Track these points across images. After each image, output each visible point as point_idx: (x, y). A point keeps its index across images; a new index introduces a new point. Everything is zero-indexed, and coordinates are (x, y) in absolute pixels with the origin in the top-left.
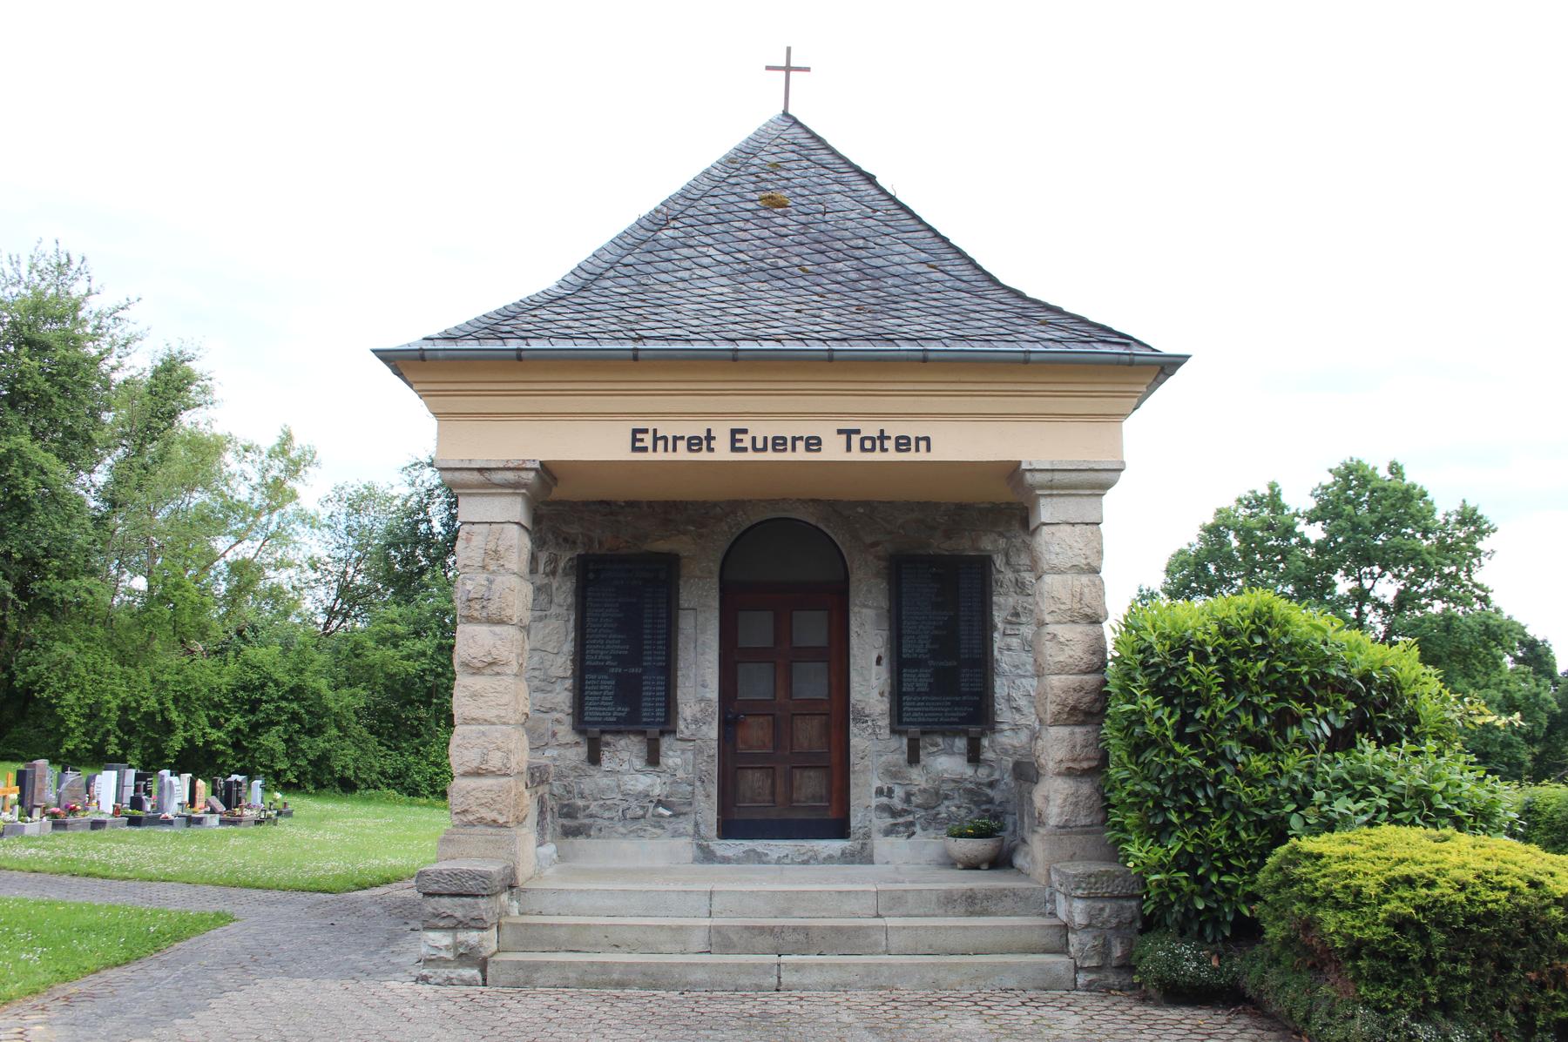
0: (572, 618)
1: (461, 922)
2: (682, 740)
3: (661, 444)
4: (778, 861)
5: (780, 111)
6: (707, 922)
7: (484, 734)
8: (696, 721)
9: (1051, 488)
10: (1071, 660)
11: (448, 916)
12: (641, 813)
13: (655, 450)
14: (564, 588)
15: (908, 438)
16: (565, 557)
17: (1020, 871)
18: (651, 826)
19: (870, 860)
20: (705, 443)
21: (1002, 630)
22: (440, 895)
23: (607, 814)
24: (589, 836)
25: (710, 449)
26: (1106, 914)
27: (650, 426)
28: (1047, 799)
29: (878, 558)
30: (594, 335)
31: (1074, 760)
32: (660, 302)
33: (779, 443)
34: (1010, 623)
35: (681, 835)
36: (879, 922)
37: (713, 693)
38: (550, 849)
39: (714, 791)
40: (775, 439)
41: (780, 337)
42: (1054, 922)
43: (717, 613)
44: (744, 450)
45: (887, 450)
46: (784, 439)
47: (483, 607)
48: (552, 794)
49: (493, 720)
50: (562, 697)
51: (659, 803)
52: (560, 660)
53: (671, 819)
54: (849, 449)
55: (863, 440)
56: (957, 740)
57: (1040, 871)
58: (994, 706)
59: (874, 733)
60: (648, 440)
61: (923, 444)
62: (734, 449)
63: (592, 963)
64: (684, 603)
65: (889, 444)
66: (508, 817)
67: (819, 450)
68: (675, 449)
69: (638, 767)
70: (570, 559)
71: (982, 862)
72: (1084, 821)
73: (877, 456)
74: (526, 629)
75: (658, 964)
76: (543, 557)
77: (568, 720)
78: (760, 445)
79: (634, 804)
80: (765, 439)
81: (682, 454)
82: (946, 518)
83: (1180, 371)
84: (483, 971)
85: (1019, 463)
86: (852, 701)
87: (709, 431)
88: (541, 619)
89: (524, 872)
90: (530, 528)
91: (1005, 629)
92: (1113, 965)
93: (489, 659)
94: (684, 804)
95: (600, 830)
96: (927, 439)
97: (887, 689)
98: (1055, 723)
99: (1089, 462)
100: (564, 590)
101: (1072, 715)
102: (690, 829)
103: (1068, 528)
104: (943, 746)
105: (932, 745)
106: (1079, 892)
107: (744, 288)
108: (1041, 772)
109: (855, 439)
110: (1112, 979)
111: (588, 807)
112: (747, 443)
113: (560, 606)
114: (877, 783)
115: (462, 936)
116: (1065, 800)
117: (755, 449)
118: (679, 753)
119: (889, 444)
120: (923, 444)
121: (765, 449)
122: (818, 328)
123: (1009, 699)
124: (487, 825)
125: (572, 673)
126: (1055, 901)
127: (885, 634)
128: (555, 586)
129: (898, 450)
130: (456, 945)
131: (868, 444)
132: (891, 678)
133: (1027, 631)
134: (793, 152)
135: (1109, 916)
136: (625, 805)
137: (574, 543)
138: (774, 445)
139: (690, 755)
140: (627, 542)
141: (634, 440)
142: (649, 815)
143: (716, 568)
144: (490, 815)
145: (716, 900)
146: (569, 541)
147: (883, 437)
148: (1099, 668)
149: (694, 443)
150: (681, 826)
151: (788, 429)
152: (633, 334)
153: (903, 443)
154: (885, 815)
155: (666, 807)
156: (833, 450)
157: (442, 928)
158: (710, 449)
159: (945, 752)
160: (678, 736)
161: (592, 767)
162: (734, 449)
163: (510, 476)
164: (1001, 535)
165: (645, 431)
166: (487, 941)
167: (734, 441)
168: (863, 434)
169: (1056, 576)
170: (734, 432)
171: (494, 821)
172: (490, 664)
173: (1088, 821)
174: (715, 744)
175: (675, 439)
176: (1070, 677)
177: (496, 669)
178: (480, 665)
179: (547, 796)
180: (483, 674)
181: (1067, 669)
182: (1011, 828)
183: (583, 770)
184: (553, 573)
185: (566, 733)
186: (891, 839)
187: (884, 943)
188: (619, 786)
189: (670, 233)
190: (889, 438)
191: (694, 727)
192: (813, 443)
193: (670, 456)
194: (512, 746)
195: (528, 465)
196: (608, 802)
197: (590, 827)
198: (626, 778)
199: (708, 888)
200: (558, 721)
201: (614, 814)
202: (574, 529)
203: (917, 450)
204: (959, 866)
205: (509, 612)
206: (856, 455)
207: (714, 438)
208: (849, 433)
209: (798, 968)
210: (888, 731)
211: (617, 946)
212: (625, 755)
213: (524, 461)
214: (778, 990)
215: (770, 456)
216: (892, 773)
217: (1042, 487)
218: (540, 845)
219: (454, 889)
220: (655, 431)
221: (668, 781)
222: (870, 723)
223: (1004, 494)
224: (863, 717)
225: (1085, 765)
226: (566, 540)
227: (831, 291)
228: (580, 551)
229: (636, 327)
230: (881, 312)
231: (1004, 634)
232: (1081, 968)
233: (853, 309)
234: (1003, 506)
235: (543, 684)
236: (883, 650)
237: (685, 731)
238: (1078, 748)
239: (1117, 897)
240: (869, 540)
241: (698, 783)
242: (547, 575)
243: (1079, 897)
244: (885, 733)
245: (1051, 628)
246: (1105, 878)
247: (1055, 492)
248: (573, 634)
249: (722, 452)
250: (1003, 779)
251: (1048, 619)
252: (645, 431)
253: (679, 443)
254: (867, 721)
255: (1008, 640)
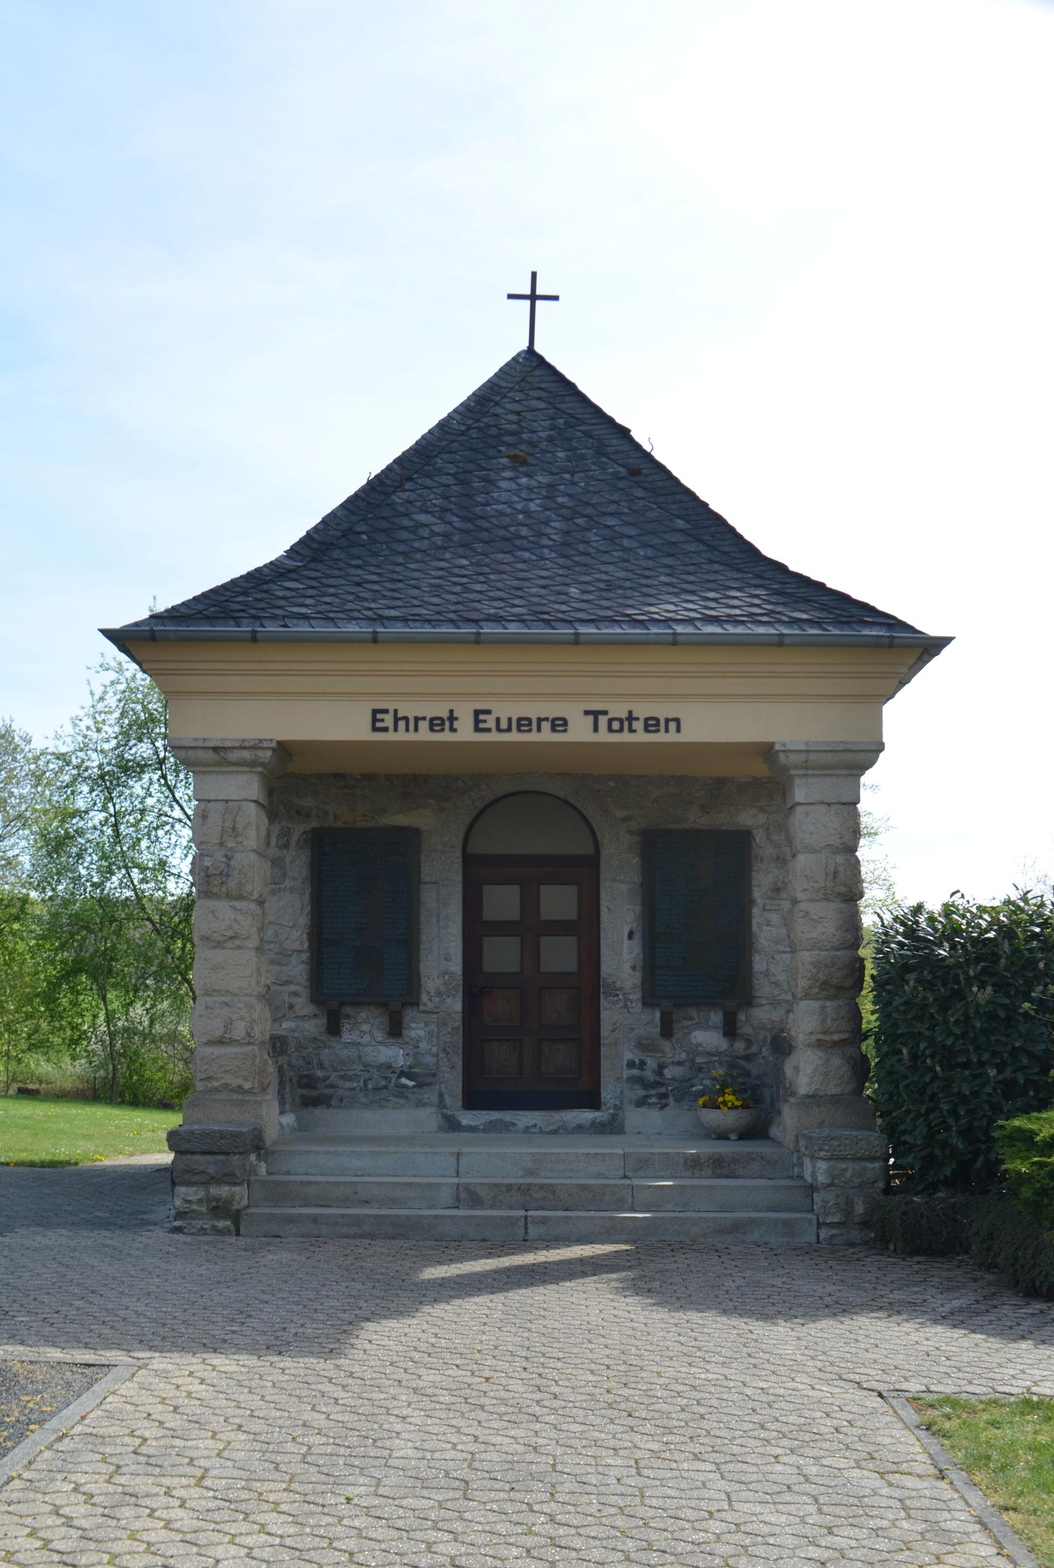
0: (308, 891)
1: (213, 1178)
2: (423, 1012)
3: (402, 724)
4: (527, 1129)
5: (525, 345)
6: (455, 1180)
7: (227, 1004)
8: (439, 994)
9: (806, 768)
10: (824, 937)
11: (201, 1172)
12: (383, 1083)
13: (396, 729)
14: (299, 861)
15: (657, 720)
16: (299, 829)
17: (773, 1140)
18: (394, 1096)
19: (620, 1131)
20: (447, 724)
21: (761, 905)
22: (193, 1153)
23: (347, 1085)
24: (329, 1106)
25: (453, 730)
26: (848, 1174)
27: (391, 707)
28: (797, 1069)
29: (631, 832)
30: (332, 615)
31: (824, 1033)
32: (395, 576)
33: (524, 724)
34: (770, 898)
35: (424, 1105)
36: (627, 1182)
37: (456, 967)
38: (289, 1119)
39: (459, 1063)
40: (519, 720)
41: (525, 617)
42: (799, 1183)
43: (459, 888)
44: (489, 730)
45: (635, 731)
46: (529, 720)
47: (222, 883)
48: (289, 1064)
49: (235, 991)
50: (298, 969)
51: (402, 1074)
52: (296, 934)
53: (415, 1090)
54: (596, 729)
55: (610, 721)
56: (712, 1014)
57: (788, 1139)
58: (751, 981)
59: (626, 1006)
60: (388, 720)
61: (672, 726)
62: (477, 729)
63: (343, 1216)
64: (425, 876)
65: (638, 725)
66: (253, 1083)
67: (565, 731)
68: (416, 729)
69: (380, 1039)
70: (304, 833)
71: (732, 1131)
72: (833, 1090)
73: (626, 737)
74: (261, 903)
75: (407, 1216)
76: (276, 829)
77: (305, 993)
78: (504, 725)
79: (375, 1075)
80: (510, 720)
81: (424, 734)
82: (704, 792)
83: (946, 651)
84: (237, 1224)
85: (772, 745)
86: (603, 974)
87: (451, 712)
88: (274, 892)
89: (271, 1135)
90: (266, 804)
91: (764, 905)
92: (856, 1221)
93: (231, 933)
94: (428, 1075)
95: (341, 1100)
96: (677, 720)
97: (640, 964)
98: (806, 996)
99: (846, 743)
100: (298, 864)
101: (824, 989)
102: (435, 1099)
103: (823, 808)
104: (697, 1020)
105: (685, 1019)
106: (822, 1154)
107: (487, 561)
108: (793, 1044)
109: (603, 720)
110: (855, 1235)
111: (328, 1078)
112: (491, 723)
113: (294, 879)
114: (628, 1056)
115: (214, 1191)
116: (815, 1071)
117: (499, 729)
118: (422, 1025)
119: (638, 725)
120: (672, 726)
121: (509, 729)
122: (564, 608)
123: (767, 974)
124: (232, 1090)
125: (309, 946)
126: (802, 1164)
127: (638, 908)
128: (288, 860)
129: (647, 730)
130: (208, 1199)
131: (616, 725)
132: (644, 952)
133: (786, 905)
134: (539, 399)
135: (852, 1176)
136: (367, 1075)
137: (308, 816)
138: (519, 726)
139: (433, 1027)
140: (364, 815)
141: (374, 720)
142: (392, 1085)
143: (458, 842)
144: (235, 1082)
145: (464, 1161)
146: (302, 814)
147: (631, 718)
148: (853, 945)
149: (436, 724)
150: (426, 1096)
151: (533, 710)
152: (370, 613)
153: (652, 724)
154: (636, 1087)
155: (410, 1077)
156: (580, 731)
157: (194, 1184)
158: (453, 730)
159: (700, 1027)
160: (422, 1008)
161: (332, 1039)
162: (477, 729)
163: (246, 755)
164: (762, 809)
165: (386, 711)
166: (239, 1194)
167: (477, 721)
168: (611, 715)
169: (810, 855)
170: (477, 713)
171: (240, 1087)
172: (231, 938)
173: (838, 1091)
174: (459, 1017)
175: (417, 719)
176: (823, 953)
177: (237, 942)
178: (220, 939)
179: (285, 1066)
180: (224, 948)
181: (819, 945)
182: (768, 1101)
183: (323, 1042)
184: (286, 846)
185: (304, 1005)
186: (643, 1110)
187: (630, 1200)
188: (360, 1057)
189: (405, 495)
190: (637, 719)
191: (437, 999)
192: (559, 724)
193: (411, 736)
194: (256, 1016)
195: (265, 745)
196: (349, 1073)
197: (331, 1097)
198: (368, 1049)
199: (456, 1150)
200: (295, 994)
201: (355, 1085)
202: (307, 802)
203: (667, 730)
204: (713, 1136)
205: (249, 888)
206: (604, 736)
207: (457, 719)
208: (596, 714)
209: (544, 1221)
210: (640, 1004)
211: (367, 1202)
212: (365, 1027)
213: (261, 741)
214: (525, 1240)
215: (515, 736)
216: (645, 1046)
217: (796, 768)
218: (282, 1113)
219: (206, 1148)
220: (396, 711)
221: (411, 1053)
222: (621, 997)
223: (760, 769)
224: (614, 991)
225: (836, 1037)
226: (298, 813)
227: (578, 564)
228: (314, 824)
229: (373, 605)
230: (631, 588)
231: (764, 909)
232: (824, 1224)
233: (602, 585)
234: (764, 780)
235: (278, 957)
236: (635, 924)
237: (429, 1003)
238: (829, 1021)
239: (861, 1159)
240: (620, 814)
241: (442, 1055)
242: (280, 848)
243: (822, 1159)
244: (637, 1007)
245: (802, 906)
246: (848, 1141)
247: (810, 772)
248: (309, 908)
249: (465, 733)
250: (761, 1052)
251: (800, 896)
252: (386, 711)
253: (421, 723)
254: (617, 995)
255: (768, 915)
